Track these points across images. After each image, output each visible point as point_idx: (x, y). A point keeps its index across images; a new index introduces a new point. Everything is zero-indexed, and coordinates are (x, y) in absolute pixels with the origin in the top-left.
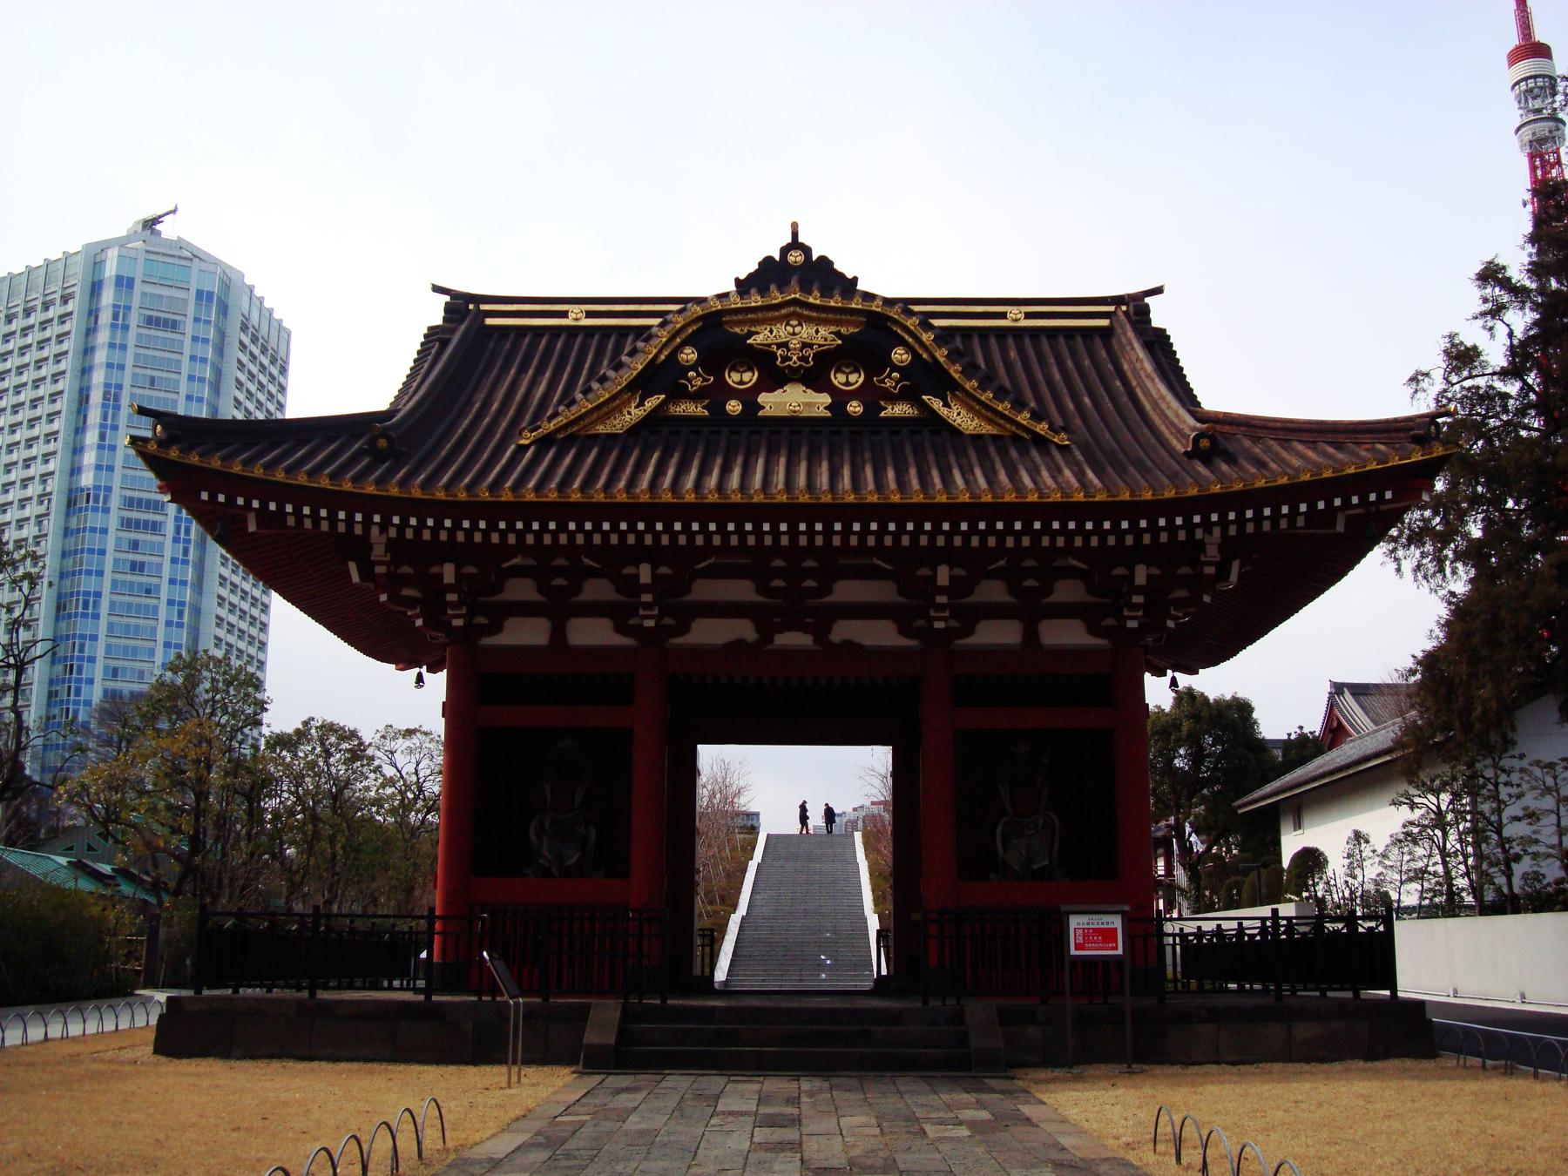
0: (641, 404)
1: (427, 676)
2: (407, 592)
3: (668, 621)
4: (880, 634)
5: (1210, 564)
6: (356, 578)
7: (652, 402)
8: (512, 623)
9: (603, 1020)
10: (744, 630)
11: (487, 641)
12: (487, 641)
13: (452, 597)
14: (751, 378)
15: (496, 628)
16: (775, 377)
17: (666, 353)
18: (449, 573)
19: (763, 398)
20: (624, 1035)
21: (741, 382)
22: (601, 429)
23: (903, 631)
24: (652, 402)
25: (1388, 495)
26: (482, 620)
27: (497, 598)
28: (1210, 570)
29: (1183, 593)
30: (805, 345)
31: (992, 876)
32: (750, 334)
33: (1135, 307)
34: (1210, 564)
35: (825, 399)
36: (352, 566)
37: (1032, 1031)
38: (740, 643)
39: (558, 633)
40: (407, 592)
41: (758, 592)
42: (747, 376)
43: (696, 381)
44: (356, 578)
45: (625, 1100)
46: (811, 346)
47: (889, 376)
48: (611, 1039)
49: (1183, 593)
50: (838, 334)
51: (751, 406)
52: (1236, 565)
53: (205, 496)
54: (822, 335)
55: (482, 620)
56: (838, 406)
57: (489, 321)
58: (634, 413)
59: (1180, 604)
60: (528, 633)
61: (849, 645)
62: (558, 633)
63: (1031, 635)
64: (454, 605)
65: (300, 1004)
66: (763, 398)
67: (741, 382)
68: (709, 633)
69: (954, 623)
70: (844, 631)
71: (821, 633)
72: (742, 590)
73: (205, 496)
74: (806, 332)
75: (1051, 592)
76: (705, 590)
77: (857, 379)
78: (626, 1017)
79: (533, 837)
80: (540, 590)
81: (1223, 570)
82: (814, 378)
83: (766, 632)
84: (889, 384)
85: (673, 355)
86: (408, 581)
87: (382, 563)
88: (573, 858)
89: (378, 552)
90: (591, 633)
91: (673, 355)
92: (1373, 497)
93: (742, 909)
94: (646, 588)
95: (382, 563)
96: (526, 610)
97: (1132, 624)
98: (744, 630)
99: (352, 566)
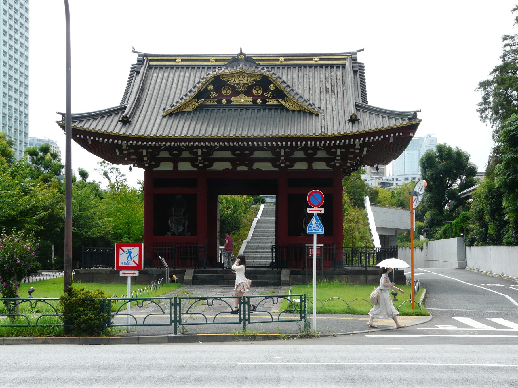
0: (197, 102)
1: (133, 168)
2: (132, 157)
3: (207, 163)
4: (267, 166)
5: (357, 149)
6: (118, 154)
7: (200, 102)
8: (162, 164)
9: (189, 274)
10: (228, 165)
11: (155, 169)
12: (155, 169)
13: (145, 159)
14: (229, 92)
15: (158, 166)
16: (236, 93)
17: (204, 87)
18: (144, 153)
19: (233, 99)
20: (194, 277)
21: (227, 93)
22: (186, 110)
23: (274, 166)
24: (200, 102)
25: (401, 134)
26: (153, 163)
27: (253, 156)
28: (357, 151)
29: (352, 156)
30: (244, 84)
31: (302, 234)
32: (228, 81)
33: (352, 57)
34: (357, 149)
35: (251, 99)
36: (117, 151)
37: (299, 276)
38: (227, 169)
39: (310, 166)
40: (132, 157)
41: (232, 154)
42: (228, 91)
43: (213, 95)
44: (118, 154)
45: (192, 290)
46: (246, 84)
47: (269, 93)
48: (191, 278)
49: (352, 156)
50: (254, 80)
51: (229, 101)
52: (365, 149)
53: (78, 136)
54: (250, 81)
55: (153, 163)
56: (254, 101)
57: (151, 63)
58: (195, 105)
59: (351, 159)
60: (166, 167)
61: (258, 169)
62: (175, 167)
63: (310, 166)
64: (145, 161)
65: (110, 270)
66: (233, 99)
67: (227, 93)
68: (218, 166)
69: (288, 163)
70: (257, 166)
71: (250, 166)
72: (228, 154)
73: (78, 136)
74: (244, 80)
75: (181, 155)
76: (217, 154)
77: (260, 92)
78: (195, 273)
79: (170, 224)
80: (170, 154)
81: (361, 150)
82: (248, 92)
83: (234, 165)
84: (269, 95)
85: (206, 88)
86: (133, 154)
87: (125, 150)
88: (181, 229)
89: (125, 147)
90: (185, 167)
91: (206, 88)
92: (397, 134)
93: (259, 216)
94: (200, 156)
95: (125, 150)
96: (300, 160)
97: (338, 164)
98: (228, 165)
99: (117, 151)
